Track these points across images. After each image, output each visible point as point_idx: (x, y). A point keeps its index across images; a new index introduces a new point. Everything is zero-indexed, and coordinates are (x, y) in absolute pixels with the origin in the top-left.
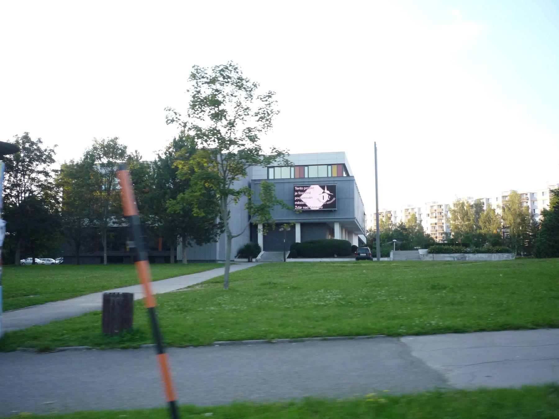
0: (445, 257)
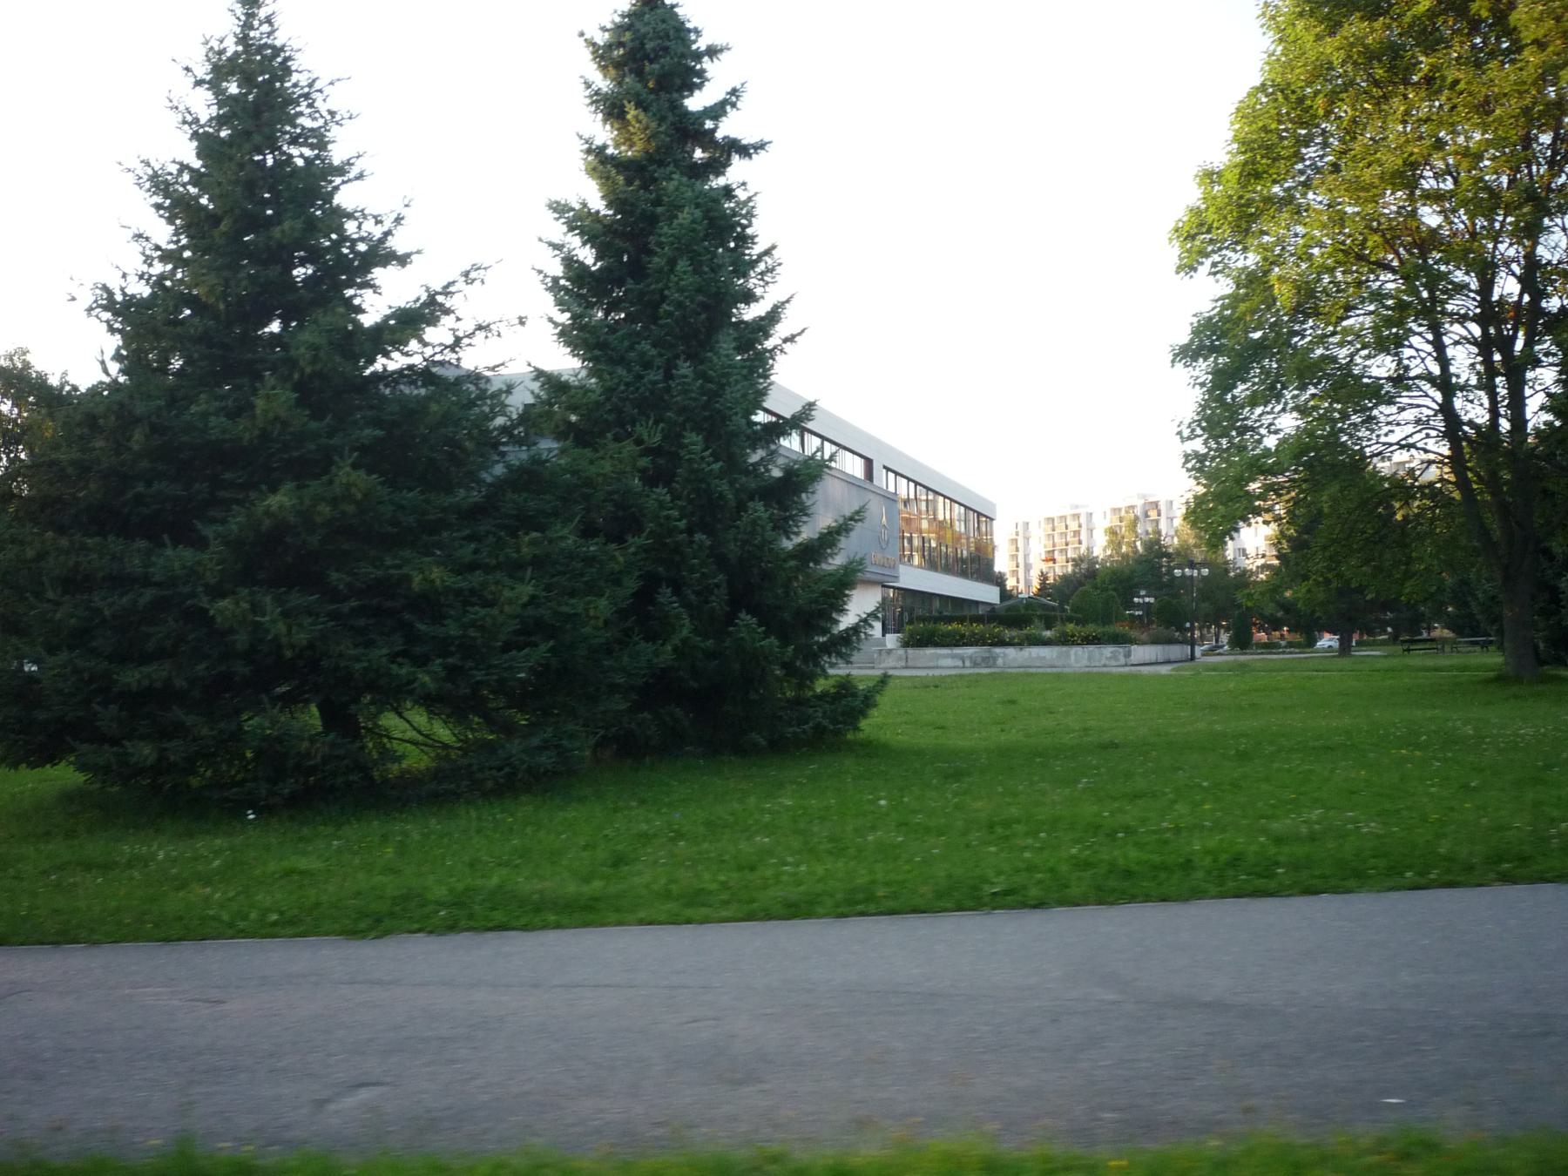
0: (939, 657)
